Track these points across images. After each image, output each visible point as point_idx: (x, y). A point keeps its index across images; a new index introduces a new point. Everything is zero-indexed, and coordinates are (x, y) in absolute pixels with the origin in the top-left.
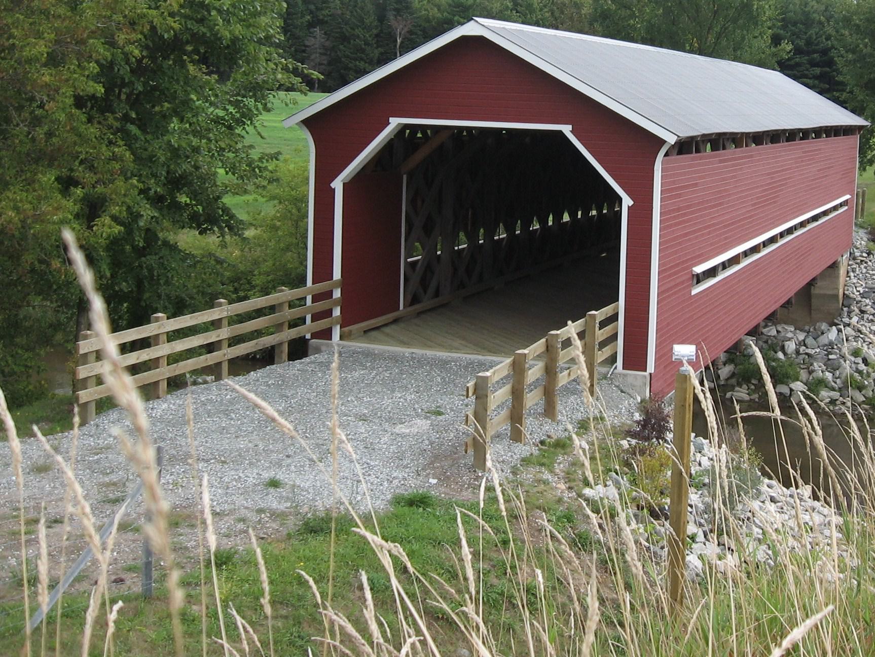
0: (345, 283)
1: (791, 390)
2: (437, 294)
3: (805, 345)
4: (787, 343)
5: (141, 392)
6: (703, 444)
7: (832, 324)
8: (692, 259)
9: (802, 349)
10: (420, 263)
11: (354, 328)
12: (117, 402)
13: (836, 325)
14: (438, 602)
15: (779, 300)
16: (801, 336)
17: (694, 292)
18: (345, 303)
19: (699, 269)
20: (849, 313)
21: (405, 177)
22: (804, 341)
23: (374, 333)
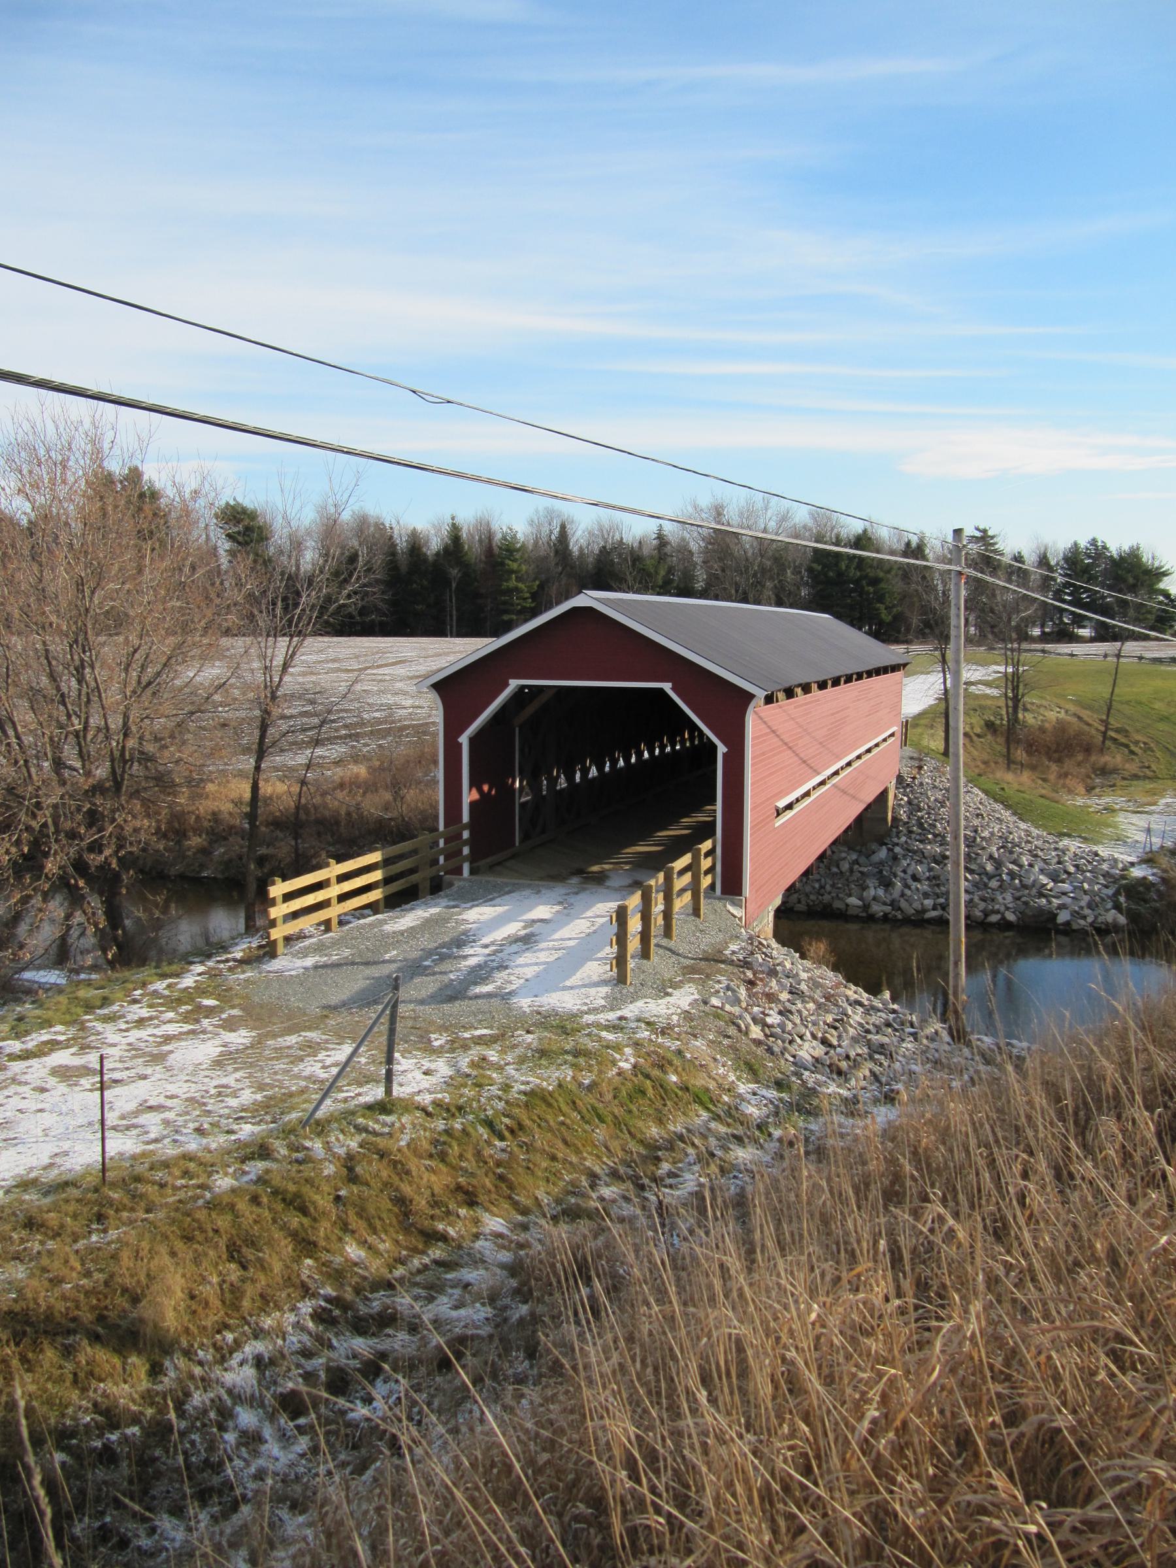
5: (491, 868)
11: (482, 863)
12: (584, 889)
14: (1137, 1346)
18: (472, 842)
19: (781, 804)
20: (899, 832)
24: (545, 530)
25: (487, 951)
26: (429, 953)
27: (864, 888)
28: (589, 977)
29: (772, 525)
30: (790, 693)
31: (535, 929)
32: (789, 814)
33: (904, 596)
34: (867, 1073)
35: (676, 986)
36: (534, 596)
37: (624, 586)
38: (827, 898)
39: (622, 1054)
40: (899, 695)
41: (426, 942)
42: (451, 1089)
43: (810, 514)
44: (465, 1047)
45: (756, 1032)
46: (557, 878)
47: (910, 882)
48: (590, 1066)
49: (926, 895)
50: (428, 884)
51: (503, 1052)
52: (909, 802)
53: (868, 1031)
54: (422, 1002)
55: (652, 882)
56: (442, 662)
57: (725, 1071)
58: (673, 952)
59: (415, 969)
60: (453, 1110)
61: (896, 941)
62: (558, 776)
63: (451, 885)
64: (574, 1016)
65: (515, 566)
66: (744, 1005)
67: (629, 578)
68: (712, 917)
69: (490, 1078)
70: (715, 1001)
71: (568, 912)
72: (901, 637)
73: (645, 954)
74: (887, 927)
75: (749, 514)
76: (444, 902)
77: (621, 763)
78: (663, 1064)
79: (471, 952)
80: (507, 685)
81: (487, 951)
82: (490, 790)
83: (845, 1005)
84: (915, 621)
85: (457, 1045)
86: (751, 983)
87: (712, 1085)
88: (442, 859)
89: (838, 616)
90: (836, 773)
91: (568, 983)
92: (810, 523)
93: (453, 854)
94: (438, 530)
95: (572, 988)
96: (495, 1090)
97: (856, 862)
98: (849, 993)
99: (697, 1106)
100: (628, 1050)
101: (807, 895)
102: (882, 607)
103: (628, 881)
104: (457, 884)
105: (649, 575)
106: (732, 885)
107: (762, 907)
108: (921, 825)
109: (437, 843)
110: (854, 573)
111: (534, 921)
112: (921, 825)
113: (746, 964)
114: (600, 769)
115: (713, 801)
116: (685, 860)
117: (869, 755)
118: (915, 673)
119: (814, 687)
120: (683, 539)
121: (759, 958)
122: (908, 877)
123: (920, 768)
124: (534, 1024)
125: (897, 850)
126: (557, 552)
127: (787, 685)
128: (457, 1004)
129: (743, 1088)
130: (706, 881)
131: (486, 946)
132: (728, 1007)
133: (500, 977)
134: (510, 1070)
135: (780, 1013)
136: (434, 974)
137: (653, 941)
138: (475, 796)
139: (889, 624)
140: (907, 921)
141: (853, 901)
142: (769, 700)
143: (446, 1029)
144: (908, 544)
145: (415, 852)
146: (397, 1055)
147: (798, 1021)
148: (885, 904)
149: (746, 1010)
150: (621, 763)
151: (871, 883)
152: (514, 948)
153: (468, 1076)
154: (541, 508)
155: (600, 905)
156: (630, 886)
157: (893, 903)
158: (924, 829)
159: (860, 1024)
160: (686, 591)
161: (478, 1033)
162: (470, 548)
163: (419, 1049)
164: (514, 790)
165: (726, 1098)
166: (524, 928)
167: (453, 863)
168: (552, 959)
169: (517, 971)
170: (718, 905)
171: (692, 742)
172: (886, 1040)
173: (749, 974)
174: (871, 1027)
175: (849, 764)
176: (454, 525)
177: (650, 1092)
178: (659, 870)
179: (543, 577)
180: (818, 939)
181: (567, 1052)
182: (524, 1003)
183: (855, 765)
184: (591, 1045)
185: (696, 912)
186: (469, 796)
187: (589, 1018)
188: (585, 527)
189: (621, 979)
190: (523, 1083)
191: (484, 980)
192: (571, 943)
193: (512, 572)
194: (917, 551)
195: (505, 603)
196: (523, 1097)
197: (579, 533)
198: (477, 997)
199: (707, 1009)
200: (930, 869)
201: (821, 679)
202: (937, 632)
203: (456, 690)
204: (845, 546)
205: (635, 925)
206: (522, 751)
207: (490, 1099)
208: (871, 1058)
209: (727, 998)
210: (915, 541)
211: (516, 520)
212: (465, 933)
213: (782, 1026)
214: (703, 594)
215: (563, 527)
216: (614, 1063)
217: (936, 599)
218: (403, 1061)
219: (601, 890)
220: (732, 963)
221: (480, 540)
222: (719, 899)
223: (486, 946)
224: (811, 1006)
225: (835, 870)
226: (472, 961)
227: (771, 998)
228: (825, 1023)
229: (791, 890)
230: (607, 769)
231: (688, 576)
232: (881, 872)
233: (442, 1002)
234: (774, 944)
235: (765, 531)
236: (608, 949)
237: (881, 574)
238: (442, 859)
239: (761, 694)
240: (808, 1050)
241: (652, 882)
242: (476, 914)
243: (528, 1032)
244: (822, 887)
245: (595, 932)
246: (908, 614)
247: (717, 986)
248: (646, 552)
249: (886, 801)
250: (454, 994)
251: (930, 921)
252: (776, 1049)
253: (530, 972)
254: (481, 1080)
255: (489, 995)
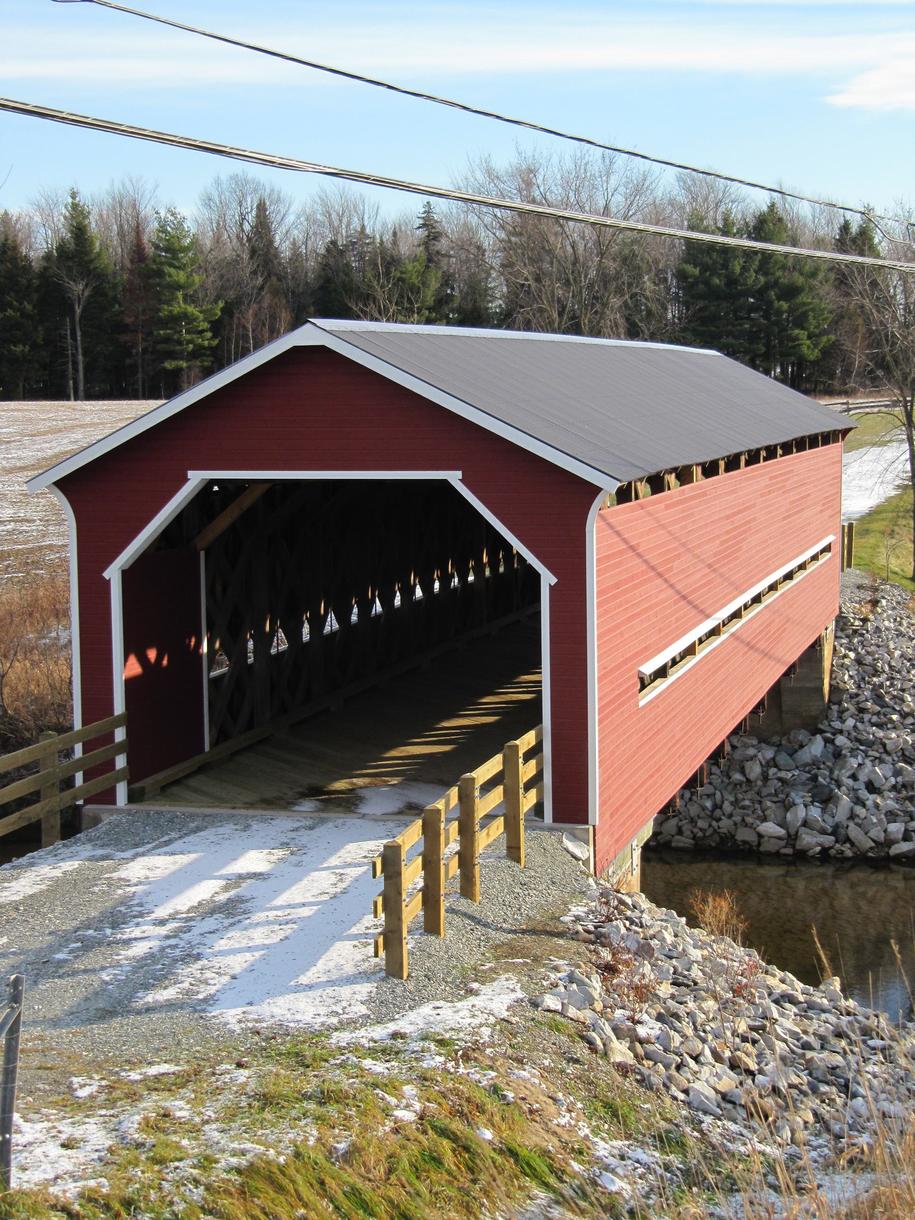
0: (129, 720)
1: (760, 836)
2: (250, 725)
3: (776, 766)
4: (748, 765)
5: (165, 791)
6: (846, 998)
7: (816, 731)
8: (636, 655)
9: (773, 771)
10: (226, 679)
12: (323, 821)
13: (821, 732)
15: (748, 703)
16: (769, 753)
17: (642, 703)
18: (131, 747)
19: (649, 668)
20: (842, 712)
21: (202, 554)
22: (774, 759)
23: (175, 789)
24: (233, 214)
25: (163, 931)
26: (64, 939)
27: (788, 806)
28: (339, 967)
29: (618, 201)
30: (657, 483)
31: (245, 889)
32: (661, 685)
33: (840, 317)
34: (810, 1118)
35: (484, 978)
36: (216, 327)
37: (371, 308)
38: (725, 824)
39: (400, 1096)
40: (838, 481)
41: (59, 920)
42: (111, 1170)
43: (679, 179)
44: (133, 1097)
45: (621, 1052)
46: (278, 803)
47: (864, 794)
48: (347, 1118)
49: (892, 816)
50: (57, 821)
51: (196, 1102)
52: (859, 661)
53: (807, 1046)
54: (55, 1023)
55: (440, 805)
56: (63, 444)
57: (570, 1119)
58: (479, 922)
59: (44, 966)
60: (117, 1206)
61: (844, 895)
62: (273, 632)
63: (96, 821)
64: (317, 1035)
65: (181, 277)
66: (599, 1006)
67: (380, 295)
68: (539, 860)
69: (178, 1147)
70: (551, 1002)
71: (299, 860)
72: (836, 384)
73: (431, 926)
74: (829, 870)
75: (578, 181)
76: (87, 850)
77: (378, 607)
78: (470, 1109)
79: (137, 933)
80: (186, 480)
81: (163, 931)
82: (159, 658)
83: (768, 1002)
84: (859, 359)
85: (119, 1094)
86: (609, 970)
87: (552, 1144)
88: (79, 778)
89: (731, 352)
90: (736, 615)
91: (304, 980)
92: (682, 198)
93: (99, 769)
94: (46, 213)
95: (310, 987)
96: (187, 1168)
97: (773, 763)
98: (772, 981)
99: (527, 1182)
100: (409, 1090)
101: (693, 821)
102: (803, 334)
103: (395, 805)
104: (106, 819)
105: (415, 290)
106: (571, 807)
107: (621, 841)
108: (878, 698)
109: (69, 753)
110: (754, 279)
111: (241, 877)
112: (878, 698)
113: (599, 938)
114: (343, 618)
115: (538, 664)
116: (492, 766)
117: (790, 584)
118: (861, 445)
119: (697, 471)
120: (466, 226)
121: (621, 925)
122: (860, 785)
123: (875, 603)
124: (249, 1052)
125: (841, 740)
126: (253, 252)
127: (653, 471)
128: (116, 1022)
129: (603, 1148)
130: (528, 801)
131: (162, 922)
132: (572, 1012)
133: (188, 973)
134: (212, 1132)
135: (660, 1018)
136: (74, 973)
137: (444, 904)
138: (134, 668)
139: (814, 363)
140: (861, 860)
141: (770, 828)
142: (624, 495)
143: (100, 1068)
144: (845, 228)
145: (29, 768)
146: (16, 1117)
147: (690, 1032)
148: (823, 832)
149: (602, 1014)
150: (378, 607)
151: (799, 797)
152: (210, 923)
153: (140, 1145)
154: (224, 178)
155: (351, 847)
156: (400, 812)
157: (836, 831)
158: (884, 705)
159: (794, 1035)
160: (474, 317)
161: (153, 1070)
162: (105, 246)
163: (54, 1104)
164: (200, 656)
165: (576, 1166)
166: (226, 889)
167: (100, 783)
168: (275, 939)
169: (216, 962)
170: (549, 839)
171: (494, 569)
172: (838, 1060)
173: (606, 955)
174: (811, 1039)
175: (757, 599)
176: (75, 206)
177: (449, 1160)
178: (449, 785)
179: (232, 294)
180: (719, 894)
181: (307, 1097)
182: (231, 1016)
183: (768, 600)
184: (346, 1083)
185: (513, 852)
186: (123, 669)
187: (342, 1038)
188: (301, 210)
189: (394, 969)
190: (234, 1154)
191: (161, 979)
192: (306, 912)
193: (179, 287)
194: (856, 239)
195: (167, 340)
196: (234, 1177)
197: (291, 218)
198: (149, 1009)
199: (538, 1014)
200: (897, 773)
201: (708, 458)
202: (897, 374)
203: (99, 491)
204: (739, 234)
205: (413, 876)
206: (210, 591)
207: (179, 1184)
208: (815, 1090)
209: (571, 995)
210: (856, 222)
211: (182, 197)
212: (125, 901)
213: (664, 1040)
214: (505, 320)
215: (262, 208)
216: (387, 1112)
217: (894, 318)
218: (25, 1126)
219: (352, 821)
220: (575, 936)
221: (121, 234)
222: (551, 829)
223: (162, 922)
224: (711, 1005)
225: (737, 776)
226: (140, 949)
227: (643, 993)
228: (734, 1033)
229: (667, 812)
230: (354, 618)
231: (476, 290)
232: (814, 778)
233: (90, 1021)
234: (644, 903)
235: (606, 211)
236: (369, 920)
237: (800, 280)
238: (79, 778)
239: (610, 487)
240: (711, 1079)
241: (440, 805)
242: (143, 869)
243: (240, 1065)
244: (716, 806)
245: (344, 892)
246: (847, 345)
247: (553, 976)
248: (404, 249)
249: (820, 660)
250: (111, 1006)
251: (899, 859)
252: (656, 1080)
253: (238, 963)
254: (161, 1152)
255: (170, 1006)
